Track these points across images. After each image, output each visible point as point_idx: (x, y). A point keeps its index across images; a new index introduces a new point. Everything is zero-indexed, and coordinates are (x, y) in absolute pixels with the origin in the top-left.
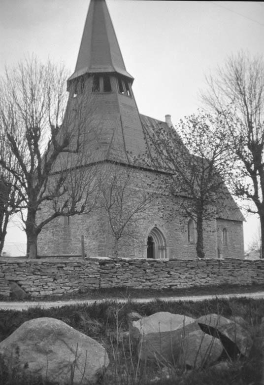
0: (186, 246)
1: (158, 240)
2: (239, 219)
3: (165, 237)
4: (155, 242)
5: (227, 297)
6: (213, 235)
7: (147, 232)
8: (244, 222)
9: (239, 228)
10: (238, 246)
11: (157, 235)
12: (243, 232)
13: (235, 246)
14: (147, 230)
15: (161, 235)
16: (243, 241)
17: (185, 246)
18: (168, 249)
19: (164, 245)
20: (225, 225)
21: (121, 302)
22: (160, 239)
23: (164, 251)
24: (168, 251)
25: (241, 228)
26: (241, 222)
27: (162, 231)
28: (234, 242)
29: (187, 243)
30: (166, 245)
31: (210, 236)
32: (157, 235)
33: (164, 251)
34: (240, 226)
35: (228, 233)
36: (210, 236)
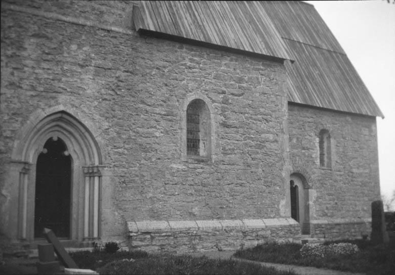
0: (181, 167)
1: (82, 150)
2: (365, 111)
3: (98, 139)
4: (74, 156)
5: (314, 34)
6: (276, 141)
7: (22, 124)
8: (378, 119)
9: (366, 132)
10: (361, 170)
11: (77, 136)
12: (376, 140)
13: (355, 170)
14: (27, 118)
15: (87, 134)
16: (375, 160)
17: (174, 166)
18: (107, 173)
19: (97, 163)
20: (327, 122)
21: (200, 225)
22: (88, 147)
23: (96, 179)
24: (106, 180)
25: (371, 131)
26: (373, 119)
27: (87, 123)
28: (351, 163)
29: (183, 159)
30: (101, 163)
31: (267, 144)
32: (77, 136)
33: (96, 179)
34: (369, 127)
35: (332, 140)
36: (267, 144)
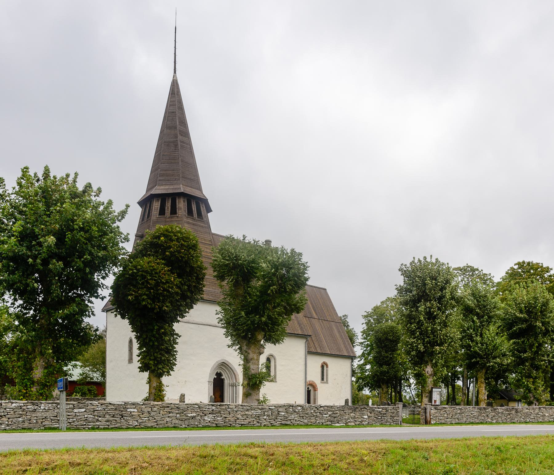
33: (235, 387)
